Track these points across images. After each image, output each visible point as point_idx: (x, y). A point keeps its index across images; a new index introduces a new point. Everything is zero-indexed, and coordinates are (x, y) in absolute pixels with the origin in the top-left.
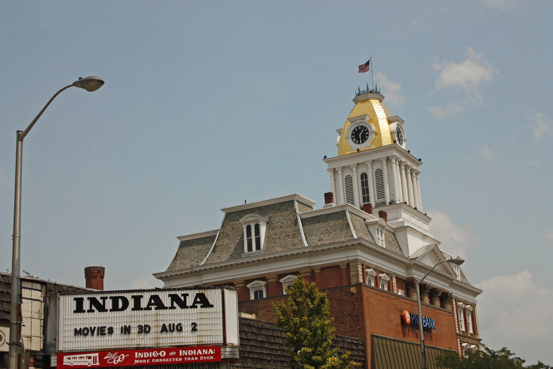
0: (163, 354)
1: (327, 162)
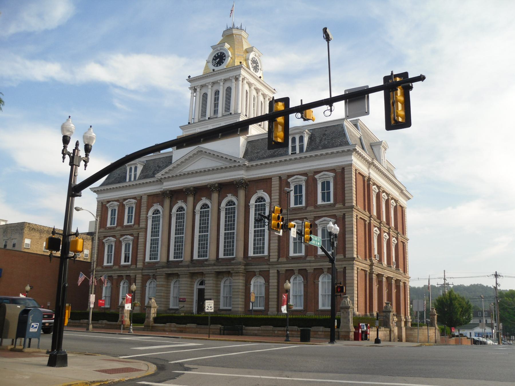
1: (189, 81)
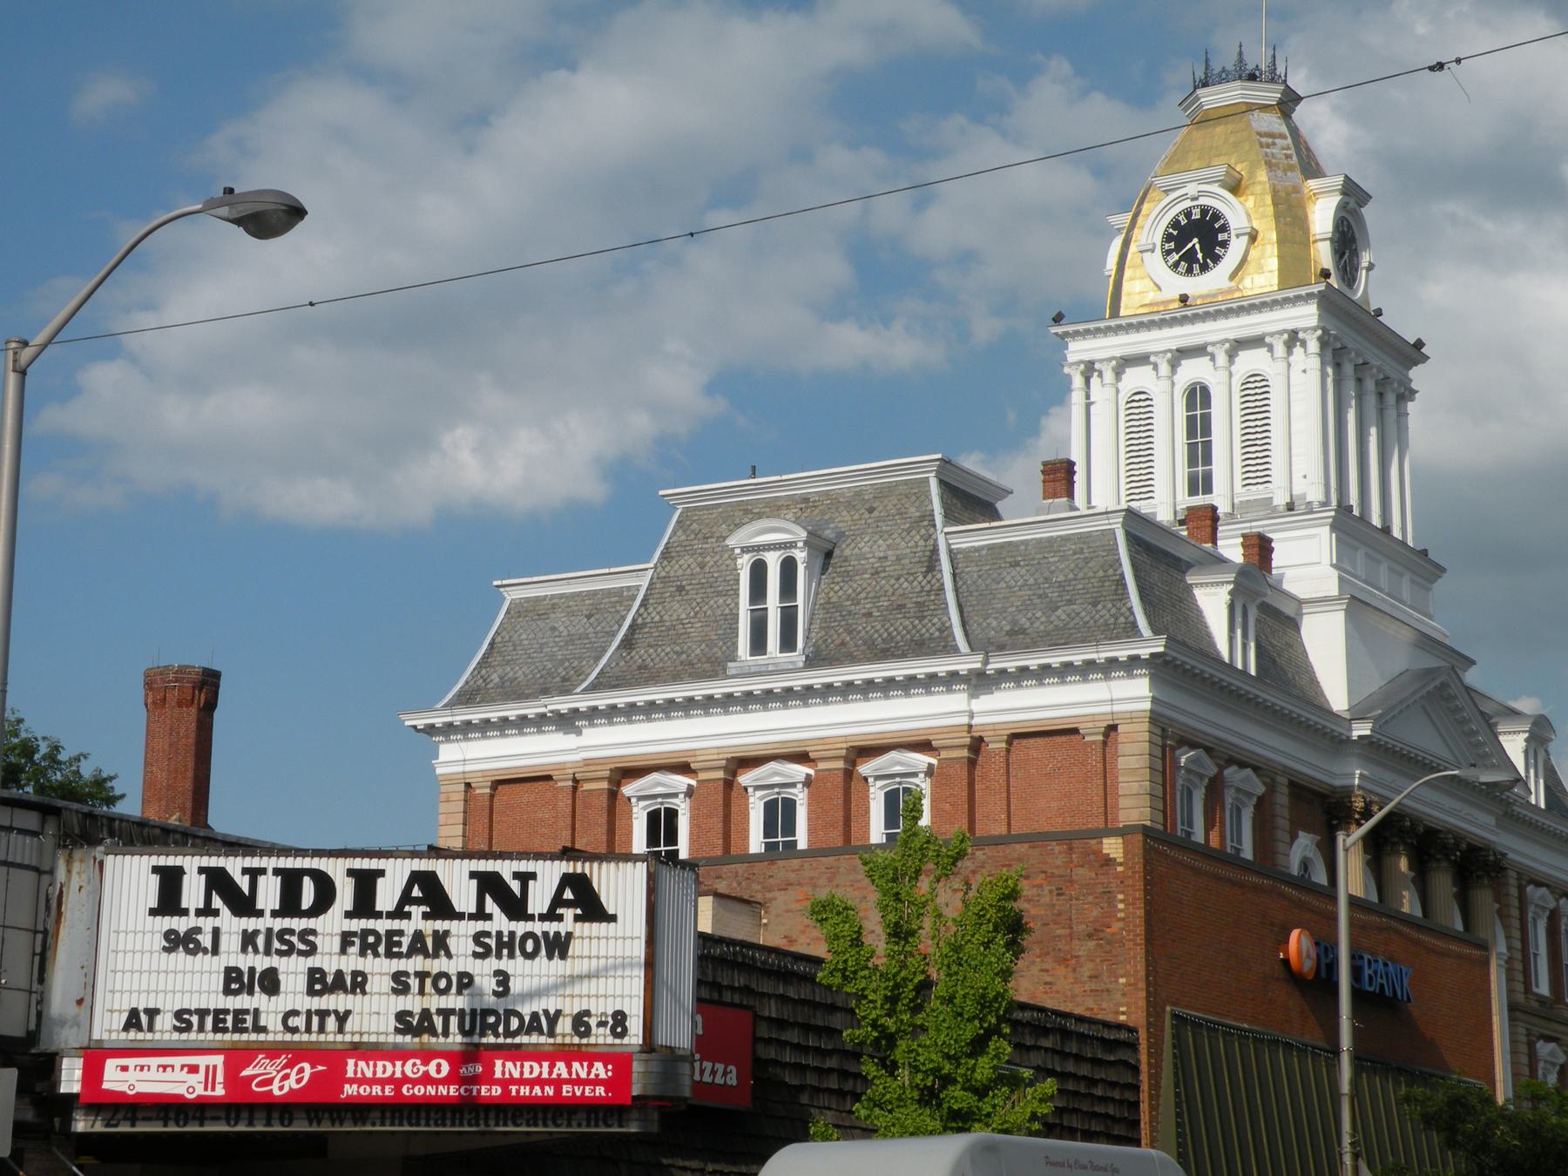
0: (439, 1071)
